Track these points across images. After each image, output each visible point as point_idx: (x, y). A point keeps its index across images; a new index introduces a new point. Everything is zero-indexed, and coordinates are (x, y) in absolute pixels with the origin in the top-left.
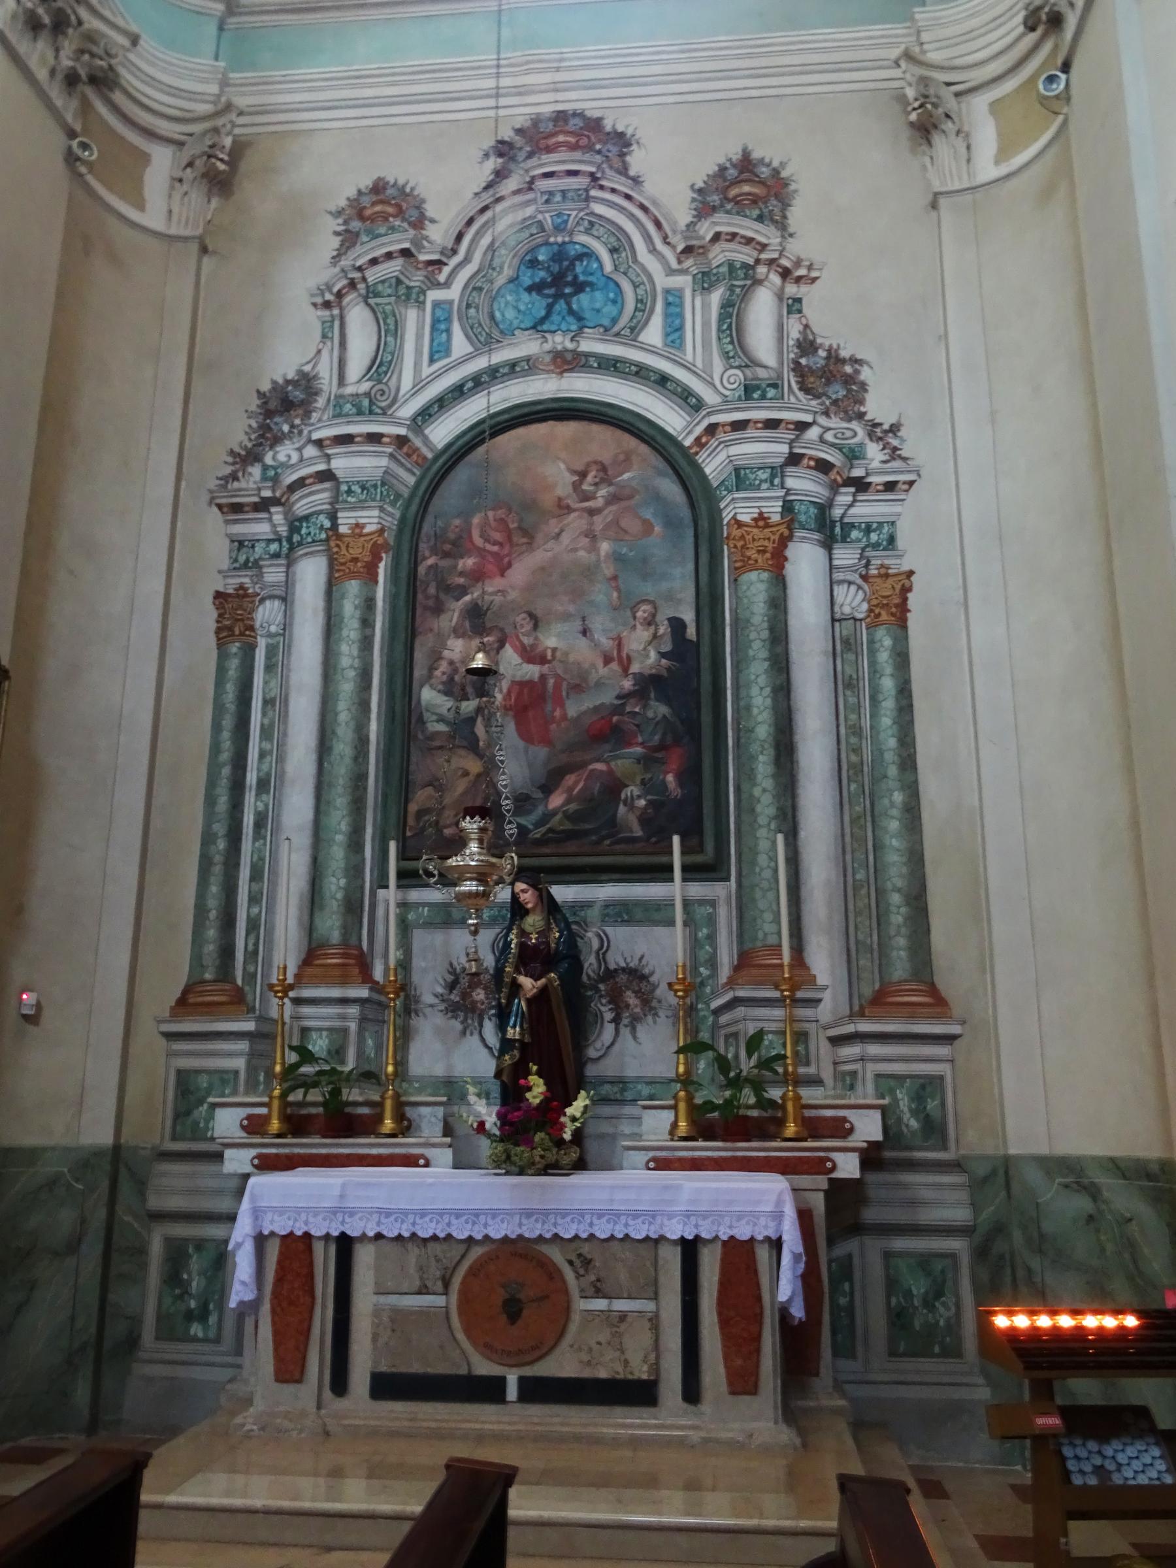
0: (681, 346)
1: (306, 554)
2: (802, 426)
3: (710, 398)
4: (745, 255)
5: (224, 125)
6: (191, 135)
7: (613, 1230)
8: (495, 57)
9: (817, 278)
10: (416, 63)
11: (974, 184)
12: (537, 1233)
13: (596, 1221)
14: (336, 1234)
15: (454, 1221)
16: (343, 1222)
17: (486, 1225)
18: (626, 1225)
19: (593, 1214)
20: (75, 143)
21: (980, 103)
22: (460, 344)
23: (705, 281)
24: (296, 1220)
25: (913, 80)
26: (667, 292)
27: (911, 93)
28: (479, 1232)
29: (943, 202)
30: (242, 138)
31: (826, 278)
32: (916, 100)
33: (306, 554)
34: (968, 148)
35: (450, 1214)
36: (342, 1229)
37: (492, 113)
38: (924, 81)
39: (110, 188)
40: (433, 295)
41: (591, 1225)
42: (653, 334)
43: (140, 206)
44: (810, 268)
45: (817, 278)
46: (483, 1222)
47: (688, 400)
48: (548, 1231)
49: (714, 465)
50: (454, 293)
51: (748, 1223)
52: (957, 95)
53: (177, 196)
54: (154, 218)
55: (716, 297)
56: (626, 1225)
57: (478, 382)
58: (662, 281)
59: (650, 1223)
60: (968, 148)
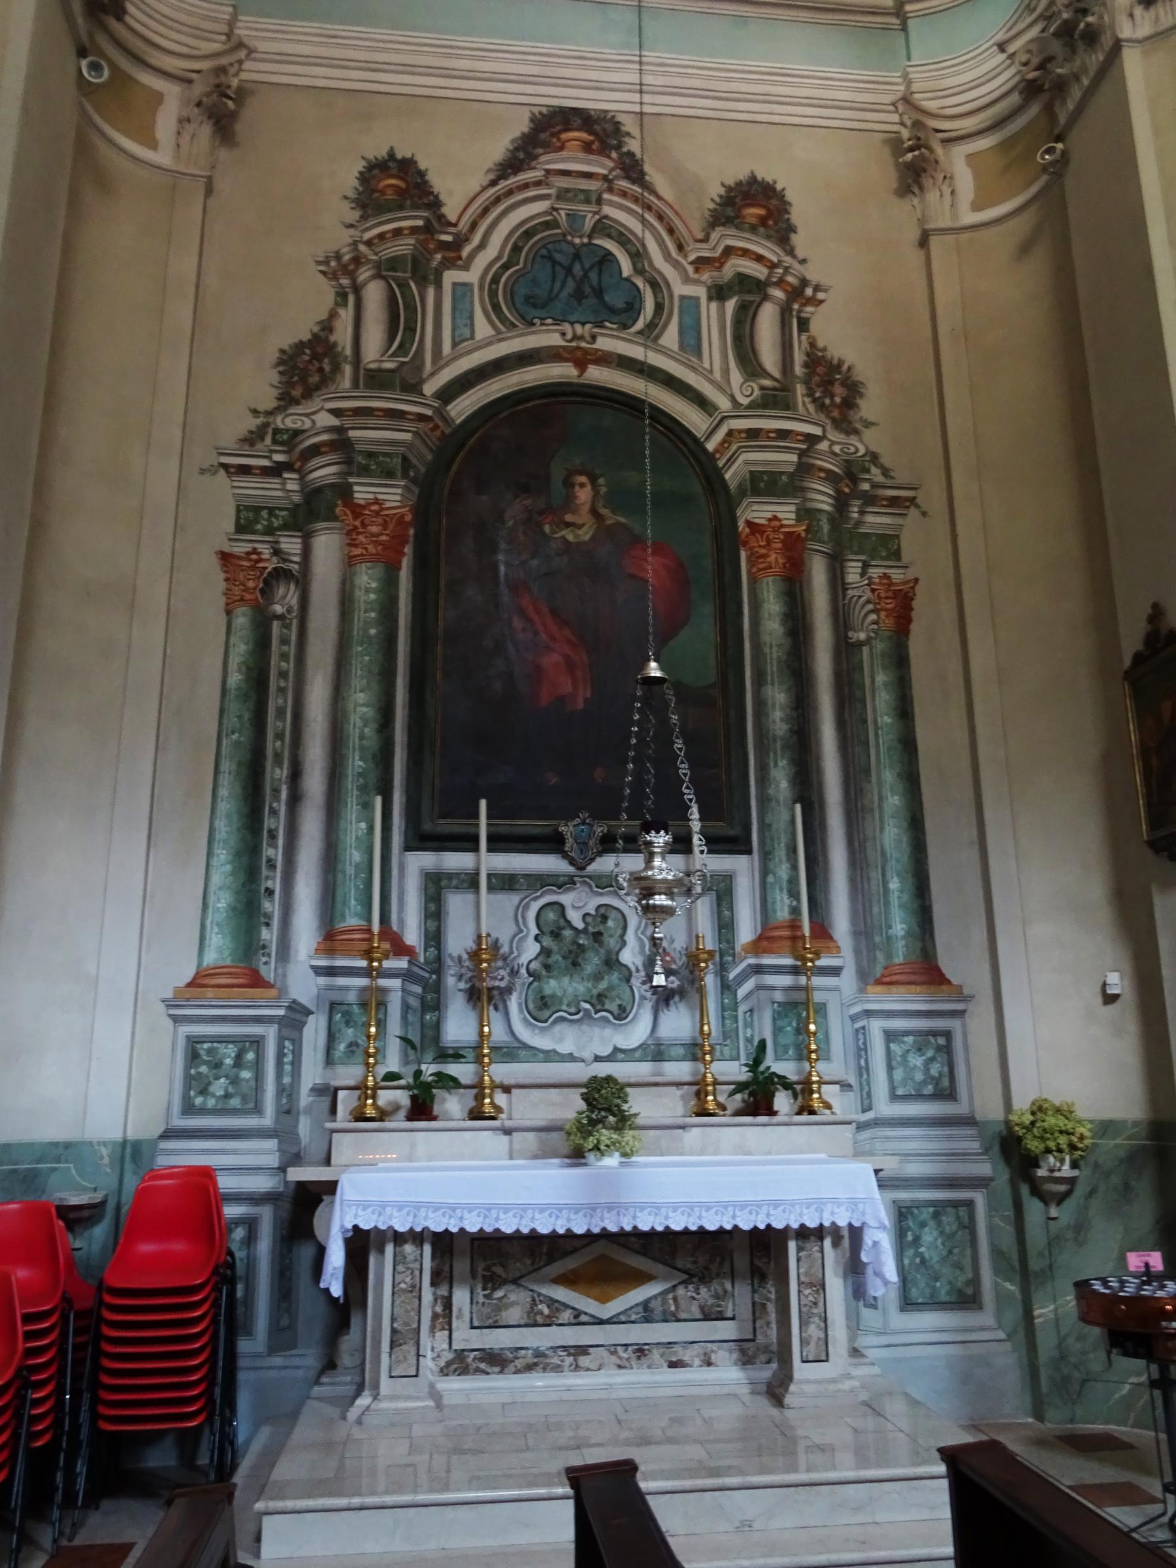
0: (698, 352)
1: (327, 529)
2: (811, 439)
3: (724, 404)
4: (758, 271)
5: (231, 65)
6: (198, 72)
7: (519, 1224)
8: (637, 53)
9: (822, 302)
10: (721, 61)
11: (957, 225)
12: (514, 1228)
13: (704, 1214)
14: (795, 1226)
15: (537, 1216)
16: (734, 1217)
17: (667, 1218)
18: (497, 1219)
19: (428, 1208)
20: (84, 63)
21: (960, 152)
22: (483, 329)
23: (719, 293)
24: (522, 1217)
25: (909, 123)
26: (683, 298)
27: (905, 133)
28: (693, 1224)
29: (934, 241)
30: (249, 85)
31: (831, 299)
32: (909, 140)
33: (327, 529)
34: (953, 192)
35: (428, 1208)
36: (533, 1226)
37: (637, 108)
38: (917, 124)
39: (107, 121)
40: (450, 277)
41: (634, 1217)
42: (670, 337)
43: (153, 145)
44: (817, 288)
45: (822, 302)
46: (530, 1216)
47: (702, 402)
48: (596, 1226)
49: (732, 475)
50: (472, 276)
51: (515, 1216)
52: (946, 141)
53: (186, 138)
54: (163, 157)
55: (731, 305)
56: (569, 1220)
57: (498, 366)
58: (680, 289)
59: (689, 1215)
60: (953, 192)
